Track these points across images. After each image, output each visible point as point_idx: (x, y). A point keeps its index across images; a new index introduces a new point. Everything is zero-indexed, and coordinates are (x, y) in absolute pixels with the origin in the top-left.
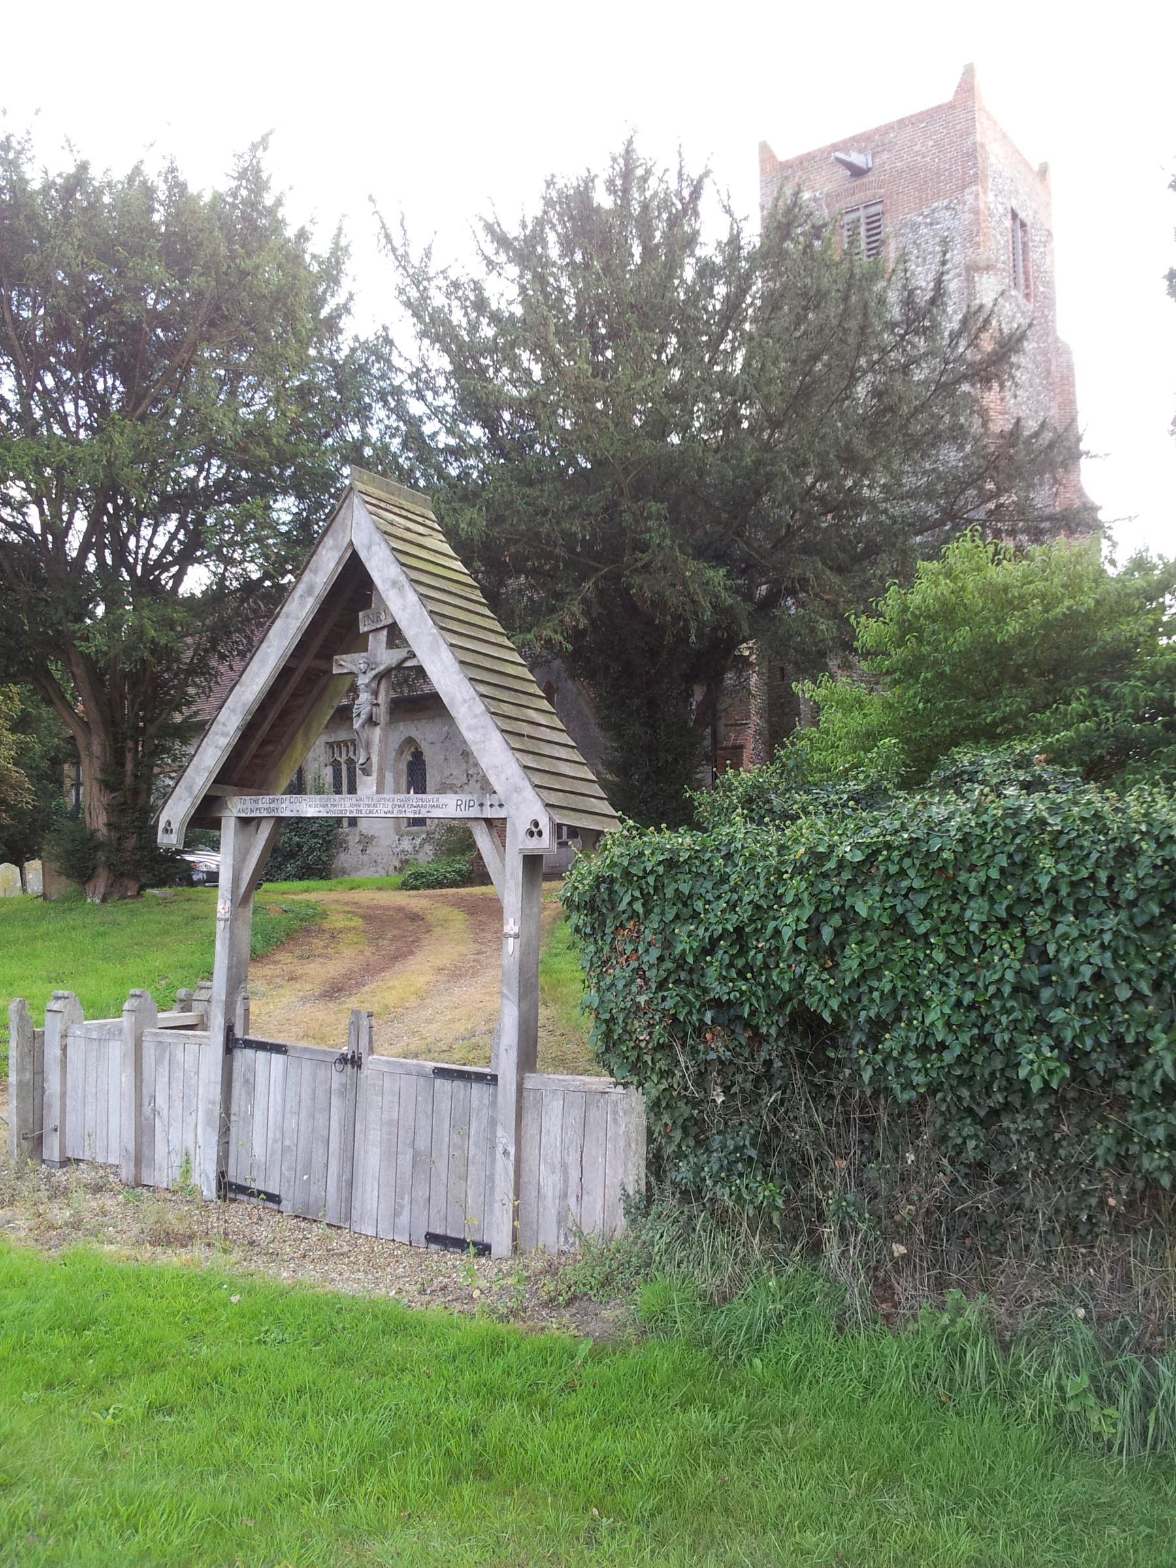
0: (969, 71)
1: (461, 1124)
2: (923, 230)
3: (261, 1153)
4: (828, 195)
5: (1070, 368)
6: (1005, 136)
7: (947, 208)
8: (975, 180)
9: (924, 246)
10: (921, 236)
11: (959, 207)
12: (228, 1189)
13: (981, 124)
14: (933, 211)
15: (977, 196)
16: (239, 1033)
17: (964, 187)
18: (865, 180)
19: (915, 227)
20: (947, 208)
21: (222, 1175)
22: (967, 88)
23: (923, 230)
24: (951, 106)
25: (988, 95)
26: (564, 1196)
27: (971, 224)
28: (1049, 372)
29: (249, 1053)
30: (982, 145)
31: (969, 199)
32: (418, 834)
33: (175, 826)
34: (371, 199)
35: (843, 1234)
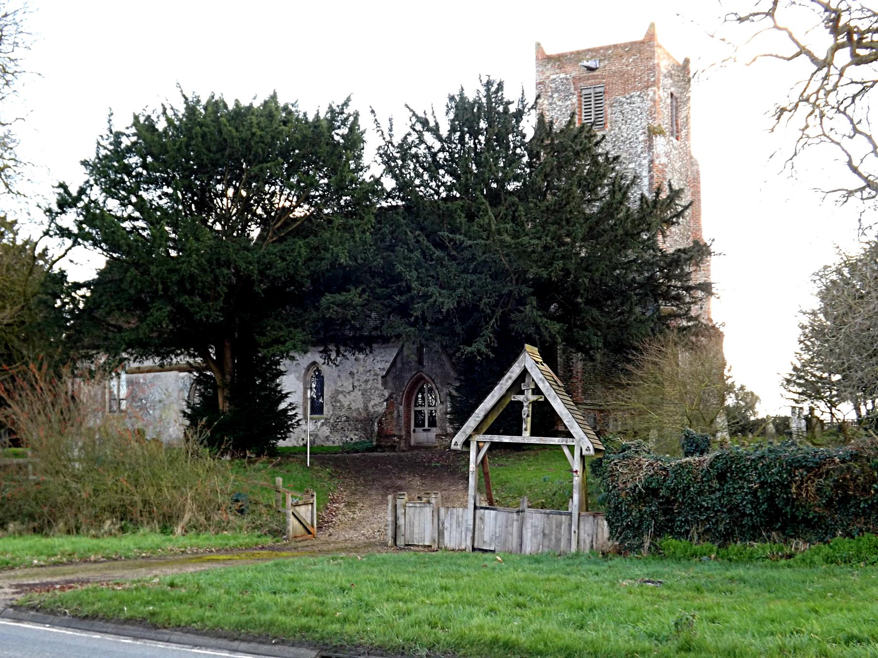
0: (652, 25)
1: (559, 526)
2: (626, 106)
3: (486, 539)
4: (574, 78)
5: (698, 173)
6: (668, 54)
7: (639, 96)
8: (654, 84)
9: (626, 114)
10: (625, 109)
11: (645, 97)
12: (474, 549)
13: (658, 51)
14: (631, 97)
15: (655, 93)
16: (478, 505)
17: (648, 87)
18: (595, 73)
19: (621, 104)
20: (639, 96)
21: (473, 546)
22: (650, 37)
23: (626, 106)
24: (642, 42)
25: (660, 39)
26: (592, 541)
27: (651, 107)
28: (687, 176)
29: (482, 511)
30: (658, 64)
31: (651, 94)
32: (319, 419)
33: (459, 443)
34: (373, 112)
35: (821, 378)
